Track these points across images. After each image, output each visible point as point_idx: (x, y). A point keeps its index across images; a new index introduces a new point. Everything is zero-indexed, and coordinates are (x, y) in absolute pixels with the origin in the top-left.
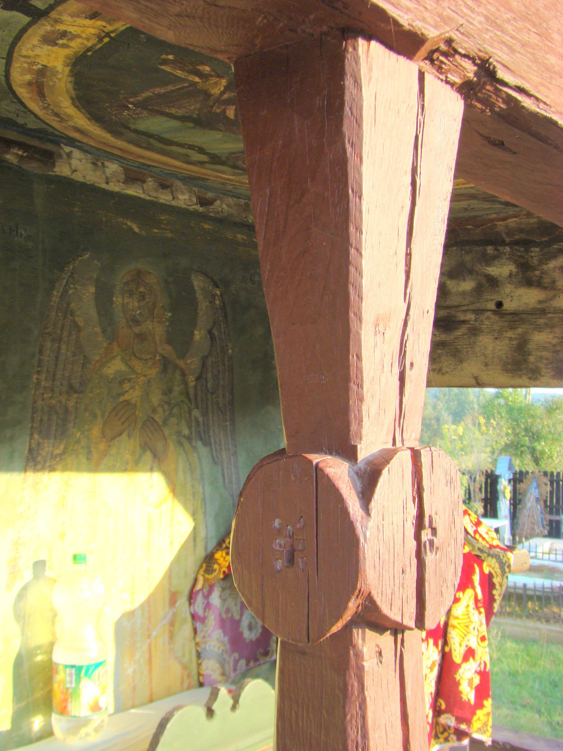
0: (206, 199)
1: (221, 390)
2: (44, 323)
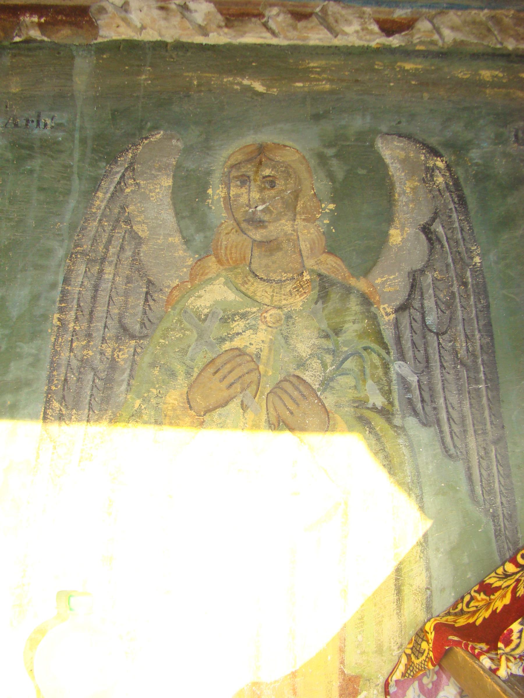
0: (393, 22)
1: (460, 327)
2: (76, 238)
